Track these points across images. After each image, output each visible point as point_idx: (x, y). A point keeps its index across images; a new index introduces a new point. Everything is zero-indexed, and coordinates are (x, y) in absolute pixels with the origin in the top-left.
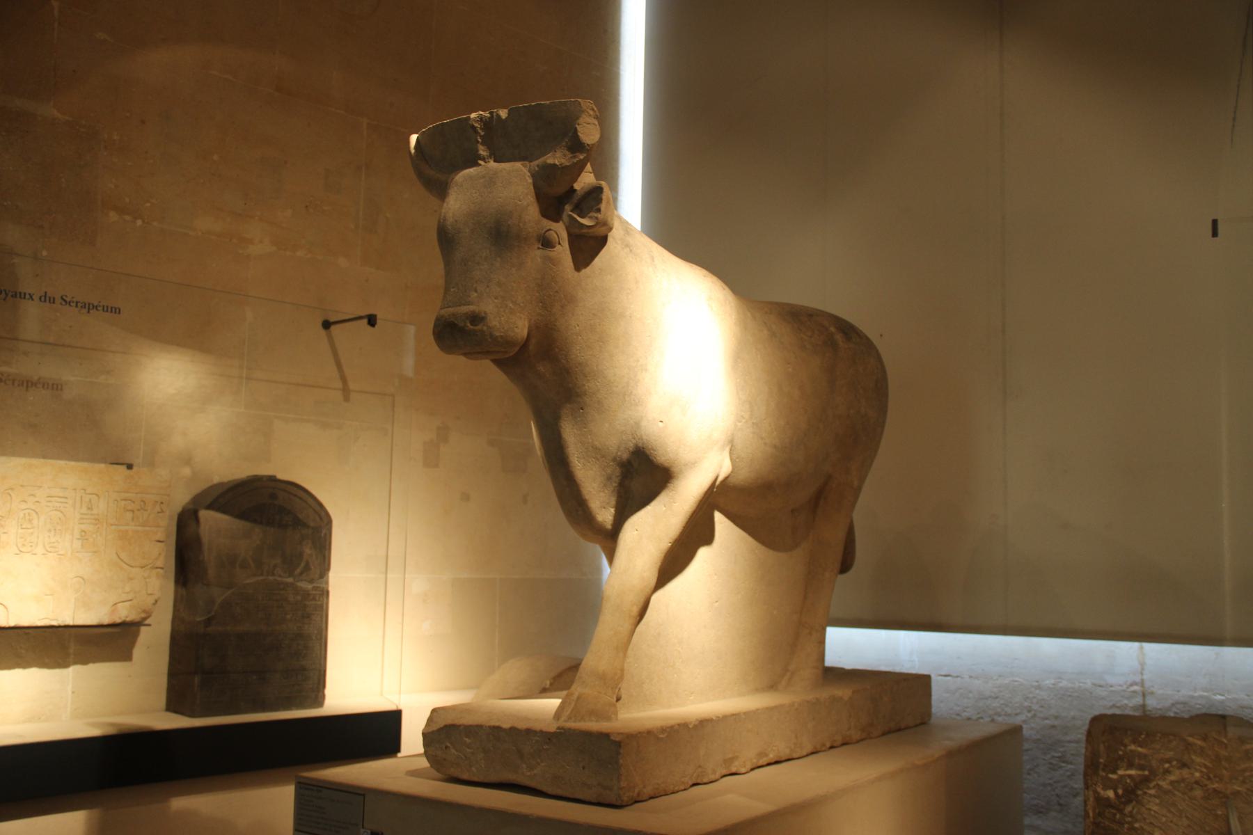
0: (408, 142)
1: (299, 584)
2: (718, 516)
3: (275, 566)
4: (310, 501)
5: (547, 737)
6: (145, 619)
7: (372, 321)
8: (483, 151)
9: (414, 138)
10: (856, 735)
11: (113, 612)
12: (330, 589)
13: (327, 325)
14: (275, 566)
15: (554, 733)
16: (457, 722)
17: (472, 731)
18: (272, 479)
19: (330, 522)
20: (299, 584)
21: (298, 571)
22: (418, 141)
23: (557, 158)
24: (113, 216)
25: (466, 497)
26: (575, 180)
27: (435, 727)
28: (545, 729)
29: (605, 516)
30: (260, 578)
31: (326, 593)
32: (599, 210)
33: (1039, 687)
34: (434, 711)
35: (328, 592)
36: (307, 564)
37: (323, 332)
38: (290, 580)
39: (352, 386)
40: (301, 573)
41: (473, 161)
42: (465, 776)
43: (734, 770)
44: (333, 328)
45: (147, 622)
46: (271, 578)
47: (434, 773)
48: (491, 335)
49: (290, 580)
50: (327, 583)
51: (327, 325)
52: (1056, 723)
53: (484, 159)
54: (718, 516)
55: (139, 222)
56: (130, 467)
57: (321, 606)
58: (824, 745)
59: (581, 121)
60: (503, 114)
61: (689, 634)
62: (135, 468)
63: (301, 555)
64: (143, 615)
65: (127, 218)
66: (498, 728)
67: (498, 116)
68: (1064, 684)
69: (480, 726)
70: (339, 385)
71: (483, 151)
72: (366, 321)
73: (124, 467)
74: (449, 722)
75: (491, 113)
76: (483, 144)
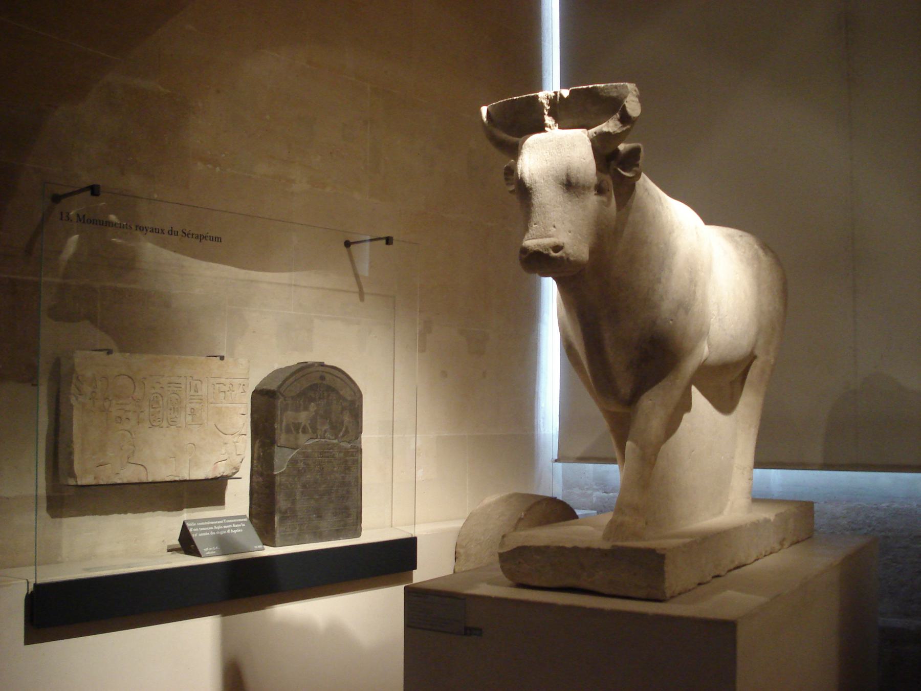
0: (481, 113)
3: (325, 431)
5: (603, 553)
6: (234, 473)
7: (389, 241)
8: (549, 120)
9: (484, 110)
10: (777, 546)
11: (215, 469)
13: (348, 244)
14: (325, 431)
16: (526, 544)
21: (341, 434)
23: (610, 126)
24: (200, 166)
25: (444, 374)
29: (625, 388)
32: (638, 165)
33: (878, 509)
36: (347, 428)
37: (344, 249)
38: (336, 441)
39: (365, 290)
40: (343, 436)
41: (540, 127)
42: (536, 584)
44: (352, 247)
47: (510, 582)
48: (568, 259)
49: (336, 441)
51: (348, 244)
52: (890, 534)
55: (218, 169)
56: (222, 358)
57: (357, 460)
59: (628, 99)
61: (723, 471)
63: (342, 423)
65: (210, 166)
66: (563, 548)
68: (896, 505)
69: (547, 547)
70: (356, 289)
71: (549, 120)
74: (520, 545)
76: (549, 115)
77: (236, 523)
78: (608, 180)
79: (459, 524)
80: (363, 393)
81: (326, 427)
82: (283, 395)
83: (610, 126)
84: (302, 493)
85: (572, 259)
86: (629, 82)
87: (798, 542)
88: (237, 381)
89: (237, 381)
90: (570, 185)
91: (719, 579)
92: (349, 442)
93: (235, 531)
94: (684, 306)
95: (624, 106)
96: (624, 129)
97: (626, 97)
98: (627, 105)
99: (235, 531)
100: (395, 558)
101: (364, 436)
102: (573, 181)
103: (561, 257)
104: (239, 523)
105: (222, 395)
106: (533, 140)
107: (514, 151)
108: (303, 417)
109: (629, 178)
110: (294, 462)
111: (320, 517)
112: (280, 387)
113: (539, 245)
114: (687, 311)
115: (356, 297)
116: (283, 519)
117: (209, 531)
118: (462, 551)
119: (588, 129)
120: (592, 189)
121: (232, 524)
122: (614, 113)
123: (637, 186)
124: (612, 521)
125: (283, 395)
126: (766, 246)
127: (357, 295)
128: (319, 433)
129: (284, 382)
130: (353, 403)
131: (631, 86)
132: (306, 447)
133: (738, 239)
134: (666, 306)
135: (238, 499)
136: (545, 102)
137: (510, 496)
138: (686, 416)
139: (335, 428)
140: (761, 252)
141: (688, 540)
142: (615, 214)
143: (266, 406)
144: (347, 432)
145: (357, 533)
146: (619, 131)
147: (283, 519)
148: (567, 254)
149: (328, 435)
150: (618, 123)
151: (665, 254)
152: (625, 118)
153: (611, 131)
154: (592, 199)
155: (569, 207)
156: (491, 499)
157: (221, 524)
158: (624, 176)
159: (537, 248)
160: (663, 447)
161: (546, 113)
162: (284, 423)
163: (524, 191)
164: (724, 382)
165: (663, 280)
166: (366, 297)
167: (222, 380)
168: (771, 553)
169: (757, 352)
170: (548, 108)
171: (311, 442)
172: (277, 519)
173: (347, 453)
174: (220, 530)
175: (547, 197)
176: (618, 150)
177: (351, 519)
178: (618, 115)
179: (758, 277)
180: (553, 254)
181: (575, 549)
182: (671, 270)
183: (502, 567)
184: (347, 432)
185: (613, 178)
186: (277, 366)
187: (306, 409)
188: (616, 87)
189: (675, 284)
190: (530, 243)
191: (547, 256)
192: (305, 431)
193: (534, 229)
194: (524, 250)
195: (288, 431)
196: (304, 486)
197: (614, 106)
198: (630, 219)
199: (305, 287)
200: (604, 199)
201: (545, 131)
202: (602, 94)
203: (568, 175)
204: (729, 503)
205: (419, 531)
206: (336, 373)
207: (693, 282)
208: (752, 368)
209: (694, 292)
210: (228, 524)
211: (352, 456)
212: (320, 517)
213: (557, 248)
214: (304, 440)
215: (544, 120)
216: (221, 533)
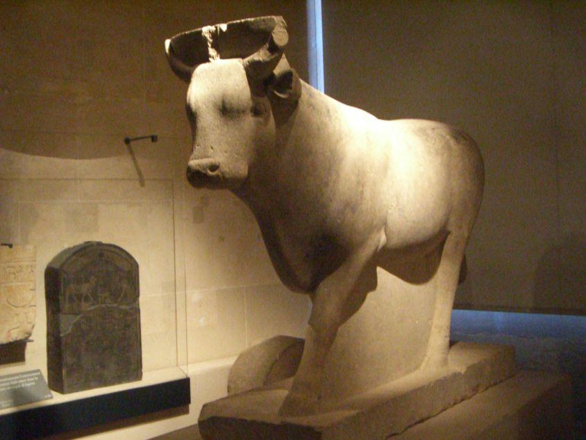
1: (120, 307)
2: (379, 269)
4: (124, 255)
7: (154, 139)
8: (212, 52)
9: (168, 43)
12: (141, 308)
15: (279, 426)
17: (227, 421)
18: (99, 244)
19: (137, 266)
20: (120, 307)
21: (120, 299)
22: (171, 45)
23: (260, 56)
25: (222, 239)
26: (274, 68)
27: (205, 418)
28: (268, 420)
29: (305, 278)
30: (98, 306)
31: (138, 311)
32: (291, 88)
34: (205, 406)
35: (139, 310)
37: (125, 146)
41: (206, 58)
43: (394, 432)
45: (31, 338)
46: (104, 305)
48: (224, 177)
49: (115, 305)
50: (138, 304)
51: (127, 141)
53: (213, 58)
54: (379, 269)
55: (6, 92)
56: (11, 246)
58: (450, 404)
59: (275, 31)
60: (224, 27)
62: (14, 247)
63: (121, 289)
64: (26, 336)
67: (221, 30)
69: (233, 419)
70: (137, 177)
71: (212, 52)
72: (150, 140)
73: (8, 247)
75: (216, 28)
76: (212, 47)
77: (30, 377)
78: (265, 102)
79: (230, 362)
80: (139, 264)
81: (107, 294)
82: (65, 273)
83: (260, 56)
84: (87, 350)
85: (227, 176)
86: (276, 15)
87: (495, 384)
88: (25, 264)
89: (25, 264)
90: (226, 110)
91: (397, 437)
92: (128, 304)
93: (29, 385)
94: (351, 206)
95: (272, 36)
96: (273, 57)
97: (273, 29)
98: (274, 35)
99: (29, 385)
100: (173, 396)
101: (142, 299)
102: (228, 106)
103: (218, 176)
104: (33, 377)
105: (12, 276)
106: (201, 69)
107: (187, 78)
108: (85, 288)
109: (284, 99)
110: (77, 325)
111: (103, 367)
112: (62, 265)
113: (199, 165)
114: (353, 210)
115: (137, 184)
116: (70, 372)
117: (5, 387)
118: (232, 386)
119: (243, 57)
120: (248, 111)
121: (26, 378)
122: (265, 44)
123: (300, 102)
124: (288, 397)
125: (65, 273)
126: (460, 134)
127: (137, 182)
128: (100, 300)
129: (67, 260)
130: (129, 272)
131: (278, 19)
132: (89, 312)
133: (429, 132)
134: (334, 206)
135: (37, 357)
136: (208, 36)
137: (281, 339)
138: (370, 295)
139: (115, 295)
140: (452, 142)
141: (353, 412)
142: (274, 131)
143: (54, 279)
144: (125, 296)
145: (138, 375)
146: (268, 60)
147: (70, 372)
148: (222, 173)
149: (108, 300)
150: (267, 52)
151: (332, 161)
152: (274, 49)
153: (261, 59)
154: (249, 121)
155: (226, 129)
156: (258, 341)
157: (17, 380)
158: (279, 98)
159: (198, 168)
160: (340, 329)
161: (209, 45)
162: (67, 294)
163: (191, 116)
164: (414, 259)
165: (331, 184)
166: (146, 182)
167: (11, 264)
168: (463, 400)
169: (450, 228)
170: (211, 40)
171: (92, 308)
172: (64, 372)
173: (126, 313)
174: (15, 385)
175: (208, 120)
176: (274, 75)
177: (133, 367)
178: (267, 45)
179: (448, 166)
180: (210, 173)
181: (253, 423)
182: (338, 174)
183: (201, 433)
184: (125, 296)
185: (272, 102)
186: (66, 246)
187: (87, 281)
188: (264, 20)
189: (344, 183)
190: (193, 163)
191: (205, 175)
192: (86, 299)
193: (198, 150)
194: (189, 169)
195: (71, 300)
196: (88, 343)
197: (263, 37)
198: (293, 133)
199: (90, 180)
200: (261, 119)
201: (209, 61)
202: (253, 27)
203: (223, 102)
204: (426, 359)
205: (192, 370)
206: (113, 249)
207: (361, 183)
208: (447, 242)
209: (362, 192)
210: (23, 379)
211: (131, 315)
212: (103, 367)
213: (214, 167)
214: (86, 307)
215: (208, 51)
216: (16, 387)
